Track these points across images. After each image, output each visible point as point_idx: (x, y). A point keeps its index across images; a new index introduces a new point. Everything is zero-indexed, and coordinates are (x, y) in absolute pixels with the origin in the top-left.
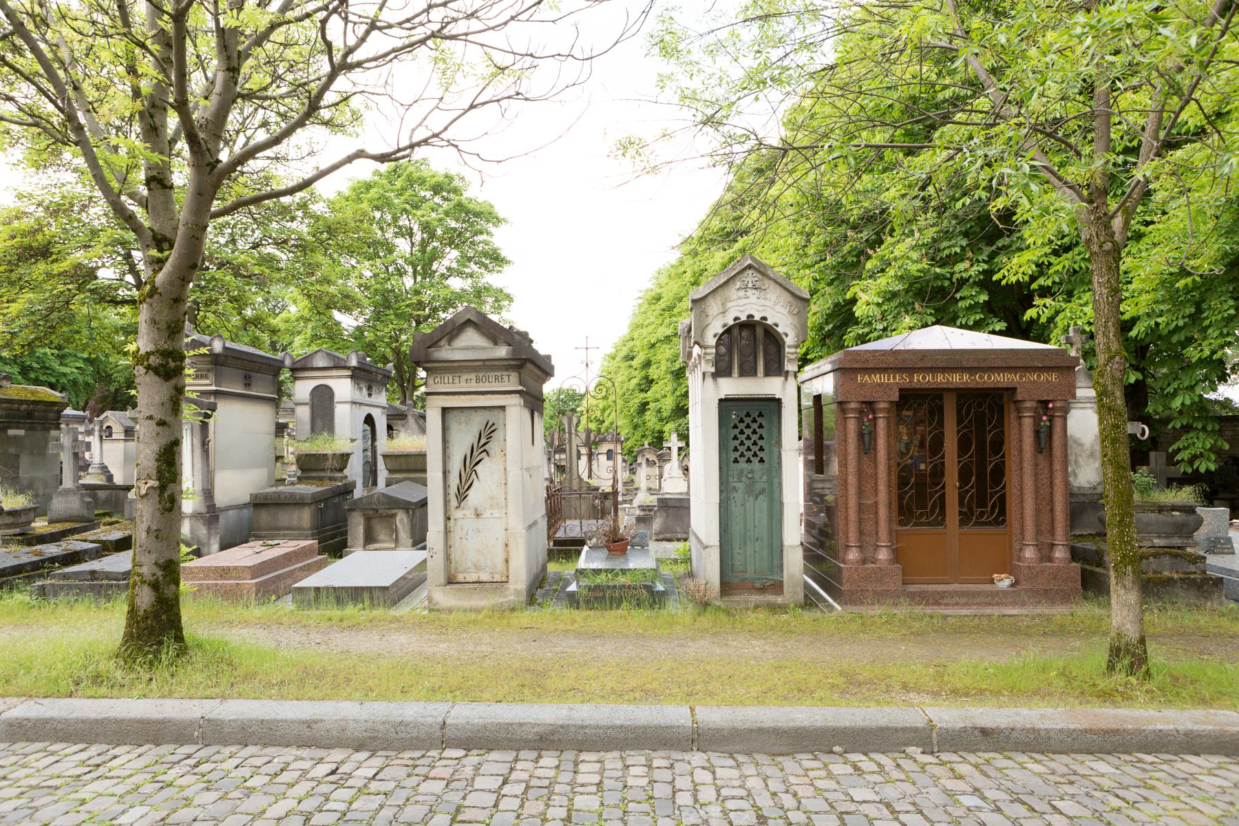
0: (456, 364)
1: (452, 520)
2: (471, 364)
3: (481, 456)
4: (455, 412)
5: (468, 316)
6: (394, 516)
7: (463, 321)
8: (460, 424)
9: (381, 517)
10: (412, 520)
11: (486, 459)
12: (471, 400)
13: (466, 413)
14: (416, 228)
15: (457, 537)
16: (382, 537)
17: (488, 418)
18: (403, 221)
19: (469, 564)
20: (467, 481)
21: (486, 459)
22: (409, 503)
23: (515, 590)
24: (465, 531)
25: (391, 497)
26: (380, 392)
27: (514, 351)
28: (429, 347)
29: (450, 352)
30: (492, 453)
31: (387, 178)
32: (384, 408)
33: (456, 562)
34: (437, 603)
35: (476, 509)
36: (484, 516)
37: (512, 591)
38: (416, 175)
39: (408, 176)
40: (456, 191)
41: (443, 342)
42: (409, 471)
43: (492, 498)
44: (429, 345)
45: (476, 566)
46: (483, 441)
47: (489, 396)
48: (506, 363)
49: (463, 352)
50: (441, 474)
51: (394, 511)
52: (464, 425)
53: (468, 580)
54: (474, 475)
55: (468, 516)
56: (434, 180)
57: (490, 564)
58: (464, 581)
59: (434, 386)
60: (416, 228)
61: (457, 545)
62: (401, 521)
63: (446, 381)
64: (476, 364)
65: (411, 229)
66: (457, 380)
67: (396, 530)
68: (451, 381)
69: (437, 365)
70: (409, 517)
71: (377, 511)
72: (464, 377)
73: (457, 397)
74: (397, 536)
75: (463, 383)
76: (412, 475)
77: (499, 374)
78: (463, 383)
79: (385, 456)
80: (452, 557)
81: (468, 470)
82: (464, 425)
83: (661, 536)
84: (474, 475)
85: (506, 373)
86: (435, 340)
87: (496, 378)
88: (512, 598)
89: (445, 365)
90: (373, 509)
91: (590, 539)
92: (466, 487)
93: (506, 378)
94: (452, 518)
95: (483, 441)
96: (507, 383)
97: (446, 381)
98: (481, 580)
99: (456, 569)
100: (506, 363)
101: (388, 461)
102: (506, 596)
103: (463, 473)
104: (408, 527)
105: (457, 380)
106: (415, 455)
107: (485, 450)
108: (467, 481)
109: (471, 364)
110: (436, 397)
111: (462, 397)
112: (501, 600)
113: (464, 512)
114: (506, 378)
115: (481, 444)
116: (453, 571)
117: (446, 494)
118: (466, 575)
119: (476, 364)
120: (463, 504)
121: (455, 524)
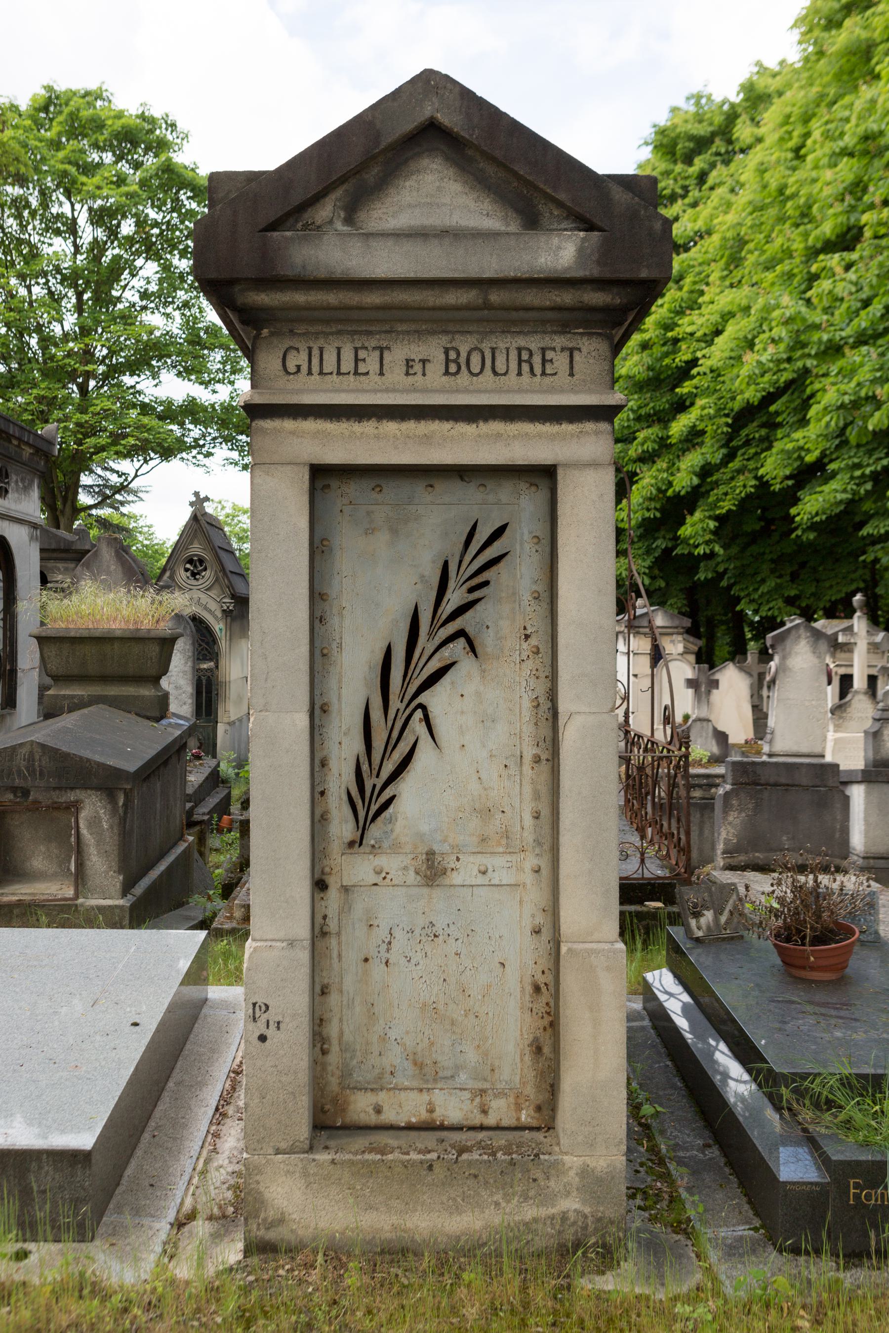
0: (374, 298)
1: (333, 893)
2: (430, 298)
3: (446, 653)
4: (353, 489)
5: (428, 110)
6: (75, 807)
7: (408, 126)
8: (370, 531)
9: (36, 807)
10: (123, 821)
11: (466, 666)
12: (427, 439)
13: (393, 490)
14: (83, 218)
15: (352, 957)
16: (38, 863)
17: (474, 513)
18: (62, 206)
19: (394, 1057)
20: (390, 746)
21: (466, 666)
22: (117, 774)
23: (585, 1172)
24: (382, 933)
25: (66, 756)
26: (27, 489)
27: (606, 254)
28: (273, 227)
29: (356, 247)
30: (487, 642)
31: (31, 117)
32: (34, 526)
33: (345, 1048)
34: (281, 1221)
35: (431, 854)
36: (456, 878)
37: (572, 1177)
38: (85, 114)
39: (71, 114)
40: (162, 145)
41: (325, 211)
42: (105, 679)
43: (486, 812)
44: (272, 214)
45: (419, 1065)
46: (455, 598)
47: (496, 426)
48: (567, 298)
49: (408, 246)
50: (302, 720)
51: (72, 796)
52: (383, 537)
53: (390, 1116)
54: (417, 726)
55: (396, 875)
56: (118, 124)
57: (472, 1057)
58: (372, 1119)
59: (283, 382)
60: (83, 218)
61: (349, 983)
62: (94, 823)
63: (330, 363)
64: (452, 298)
65: (74, 220)
66: (371, 363)
67: (79, 849)
68: (347, 365)
69: (300, 298)
70: (114, 810)
71: (26, 793)
72: (398, 354)
73: (369, 427)
74: (80, 865)
75: (396, 374)
76: (113, 691)
77: (534, 343)
78: (396, 374)
79: (42, 640)
80: (332, 1030)
81: (395, 703)
82: (383, 537)
83: (742, 858)
84: (417, 726)
85: (559, 341)
86: (297, 198)
87: (524, 359)
88: (571, 1204)
89: (332, 298)
90: (14, 789)
91: (697, 915)
92: (389, 767)
93: (561, 361)
94: (333, 883)
95: (455, 598)
96: (563, 377)
97: (330, 363)
98: (438, 1116)
99: (346, 1073)
100: (567, 298)
101: (52, 651)
102: (548, 1199)
103: (376, 715)
104: (111, 840)
105: (371, 363)
106: (122, 639)
107: (461, 633)
108: (390, 746)
109: (430, 298)
110: (289, 424)
111: (391, 427)
112: (530, 1212)
113: (382, 861)
114: (561, 361)
115: (448, 608)
116: (334, 1083)
117: (318, 794)
118: (382, 1097)
119: (452, 298)
120: (375, 831)
121: (346, 908)
